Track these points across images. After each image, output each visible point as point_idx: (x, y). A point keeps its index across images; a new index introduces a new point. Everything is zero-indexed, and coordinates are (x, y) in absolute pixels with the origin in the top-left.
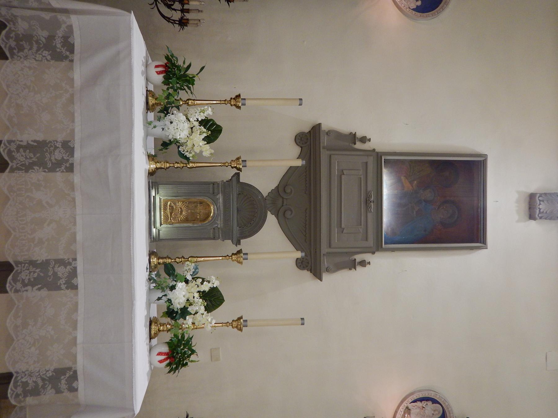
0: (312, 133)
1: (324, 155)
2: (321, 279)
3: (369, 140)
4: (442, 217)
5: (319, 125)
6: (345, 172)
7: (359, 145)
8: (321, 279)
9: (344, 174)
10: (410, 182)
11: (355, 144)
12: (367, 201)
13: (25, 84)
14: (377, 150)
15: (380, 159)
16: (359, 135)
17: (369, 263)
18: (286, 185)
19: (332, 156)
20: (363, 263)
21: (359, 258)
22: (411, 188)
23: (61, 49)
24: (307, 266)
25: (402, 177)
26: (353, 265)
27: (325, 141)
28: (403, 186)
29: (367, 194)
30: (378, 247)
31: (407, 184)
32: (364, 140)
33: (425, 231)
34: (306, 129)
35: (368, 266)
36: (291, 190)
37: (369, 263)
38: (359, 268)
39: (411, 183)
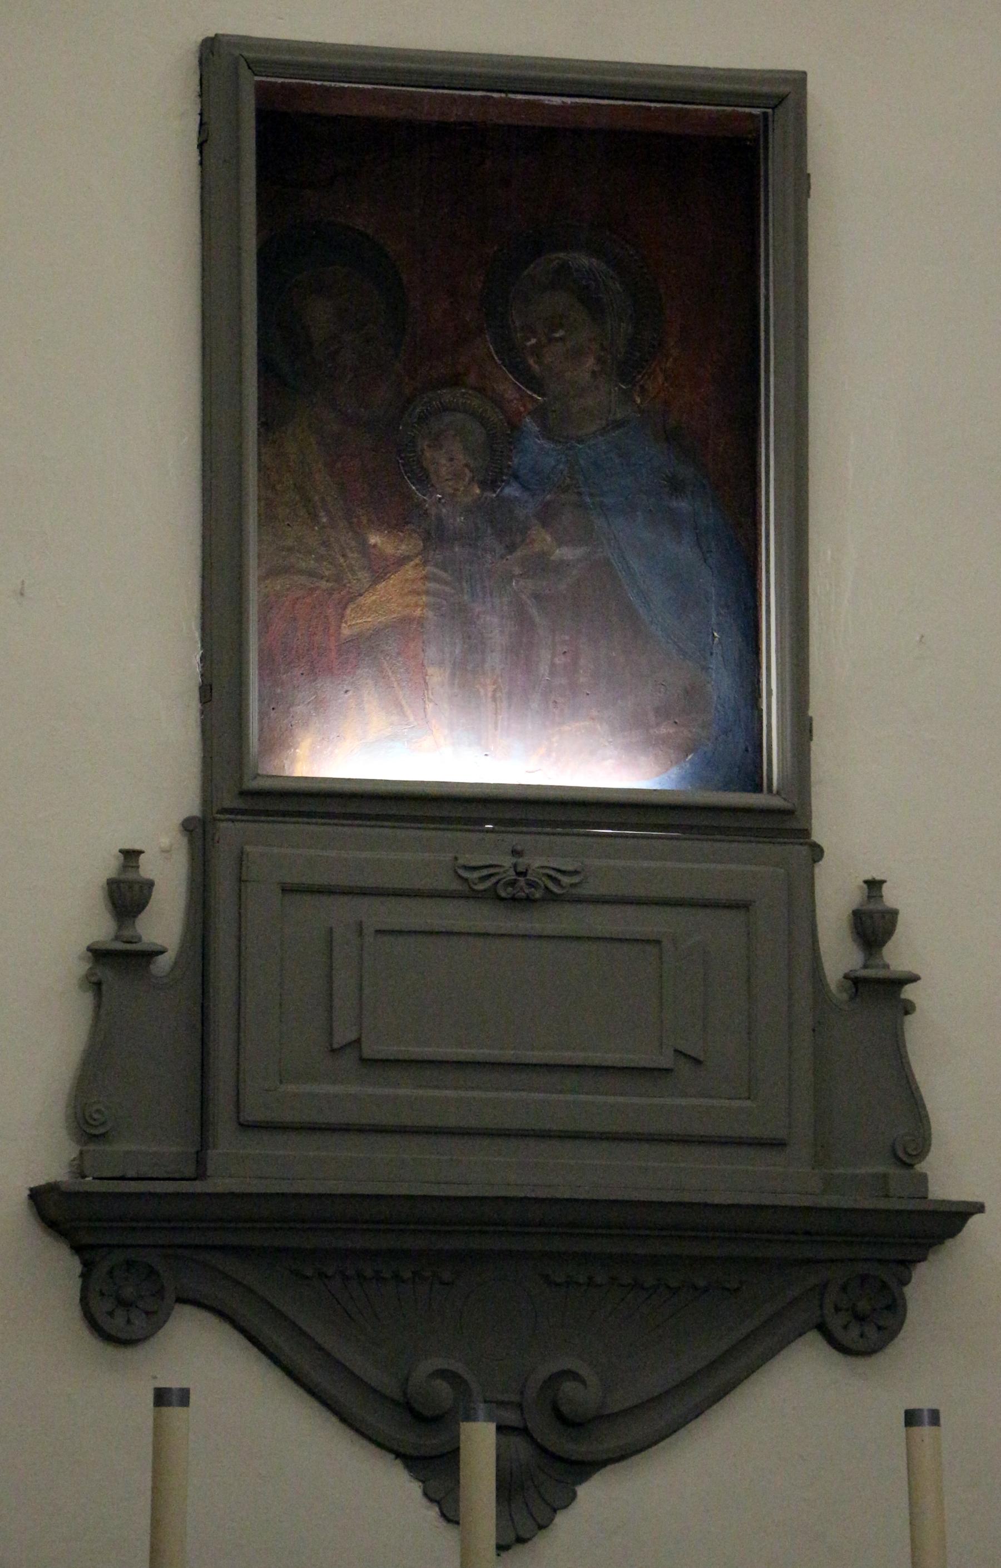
0: (87, 1239)
1: (241, 1167)
2: (955, 1218)
3: (131, 856)
4: (590, 362)
5: (41, 1199)
6: (344, 1034)
7: (163, 924)
8: (955, 1218)
9: (358, 1041)
10: (379, 576)
11: (151, 954)
12: (518, 893)
13: (458, 490)
14: (190, 805)
15: (243, 802)
16: (99, 927)
17: (874, 886)
18: (409, 1408)
19: (253, 1113)
20: (873, 926)
21: (839, 956)
22: (409, 571)
23: (657, 776)
24: (884, 1286)
25: (374, 539)
26: (883, 993)
27: (149, 1150)
28: (406, 628)
29: (473, 895)
30: (783, 827)
31: (384, 601)
32: (127, 896)
33: (676, 487)
34: (59, 1269)
35: (891, 897)
36: (442, 1374)
37: (874, 886)
38: (899, 956)
39: (380, 570)
